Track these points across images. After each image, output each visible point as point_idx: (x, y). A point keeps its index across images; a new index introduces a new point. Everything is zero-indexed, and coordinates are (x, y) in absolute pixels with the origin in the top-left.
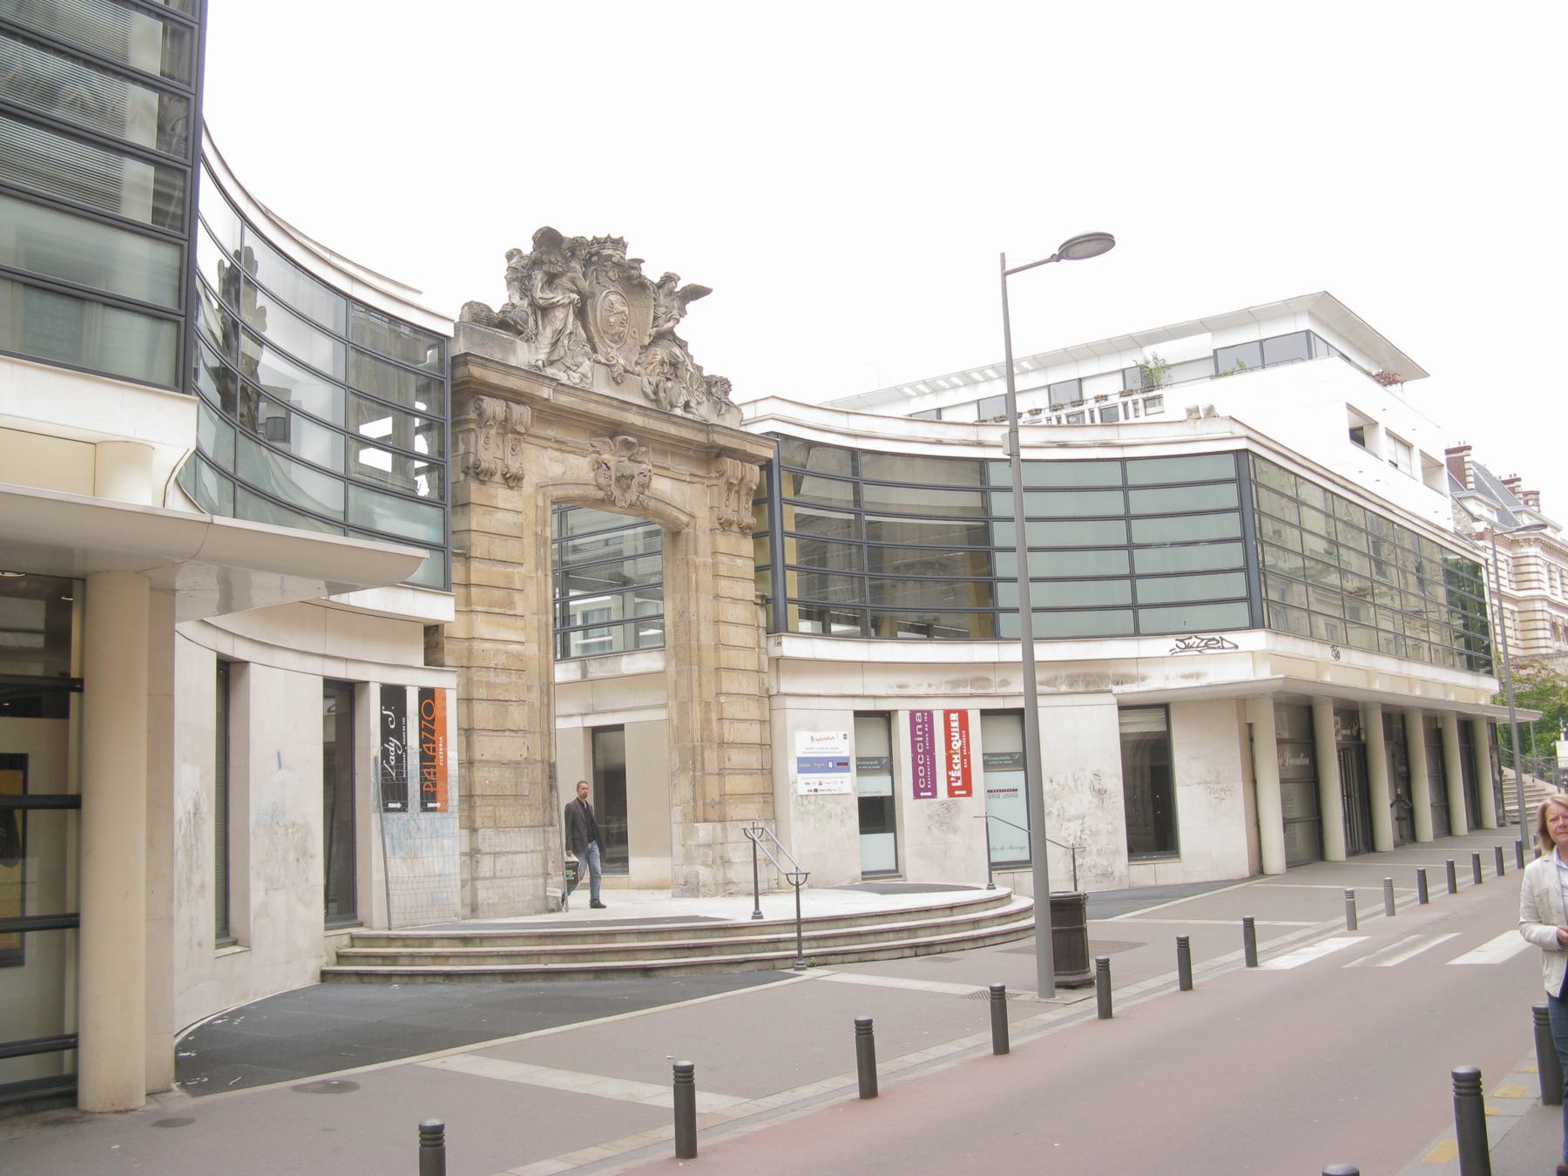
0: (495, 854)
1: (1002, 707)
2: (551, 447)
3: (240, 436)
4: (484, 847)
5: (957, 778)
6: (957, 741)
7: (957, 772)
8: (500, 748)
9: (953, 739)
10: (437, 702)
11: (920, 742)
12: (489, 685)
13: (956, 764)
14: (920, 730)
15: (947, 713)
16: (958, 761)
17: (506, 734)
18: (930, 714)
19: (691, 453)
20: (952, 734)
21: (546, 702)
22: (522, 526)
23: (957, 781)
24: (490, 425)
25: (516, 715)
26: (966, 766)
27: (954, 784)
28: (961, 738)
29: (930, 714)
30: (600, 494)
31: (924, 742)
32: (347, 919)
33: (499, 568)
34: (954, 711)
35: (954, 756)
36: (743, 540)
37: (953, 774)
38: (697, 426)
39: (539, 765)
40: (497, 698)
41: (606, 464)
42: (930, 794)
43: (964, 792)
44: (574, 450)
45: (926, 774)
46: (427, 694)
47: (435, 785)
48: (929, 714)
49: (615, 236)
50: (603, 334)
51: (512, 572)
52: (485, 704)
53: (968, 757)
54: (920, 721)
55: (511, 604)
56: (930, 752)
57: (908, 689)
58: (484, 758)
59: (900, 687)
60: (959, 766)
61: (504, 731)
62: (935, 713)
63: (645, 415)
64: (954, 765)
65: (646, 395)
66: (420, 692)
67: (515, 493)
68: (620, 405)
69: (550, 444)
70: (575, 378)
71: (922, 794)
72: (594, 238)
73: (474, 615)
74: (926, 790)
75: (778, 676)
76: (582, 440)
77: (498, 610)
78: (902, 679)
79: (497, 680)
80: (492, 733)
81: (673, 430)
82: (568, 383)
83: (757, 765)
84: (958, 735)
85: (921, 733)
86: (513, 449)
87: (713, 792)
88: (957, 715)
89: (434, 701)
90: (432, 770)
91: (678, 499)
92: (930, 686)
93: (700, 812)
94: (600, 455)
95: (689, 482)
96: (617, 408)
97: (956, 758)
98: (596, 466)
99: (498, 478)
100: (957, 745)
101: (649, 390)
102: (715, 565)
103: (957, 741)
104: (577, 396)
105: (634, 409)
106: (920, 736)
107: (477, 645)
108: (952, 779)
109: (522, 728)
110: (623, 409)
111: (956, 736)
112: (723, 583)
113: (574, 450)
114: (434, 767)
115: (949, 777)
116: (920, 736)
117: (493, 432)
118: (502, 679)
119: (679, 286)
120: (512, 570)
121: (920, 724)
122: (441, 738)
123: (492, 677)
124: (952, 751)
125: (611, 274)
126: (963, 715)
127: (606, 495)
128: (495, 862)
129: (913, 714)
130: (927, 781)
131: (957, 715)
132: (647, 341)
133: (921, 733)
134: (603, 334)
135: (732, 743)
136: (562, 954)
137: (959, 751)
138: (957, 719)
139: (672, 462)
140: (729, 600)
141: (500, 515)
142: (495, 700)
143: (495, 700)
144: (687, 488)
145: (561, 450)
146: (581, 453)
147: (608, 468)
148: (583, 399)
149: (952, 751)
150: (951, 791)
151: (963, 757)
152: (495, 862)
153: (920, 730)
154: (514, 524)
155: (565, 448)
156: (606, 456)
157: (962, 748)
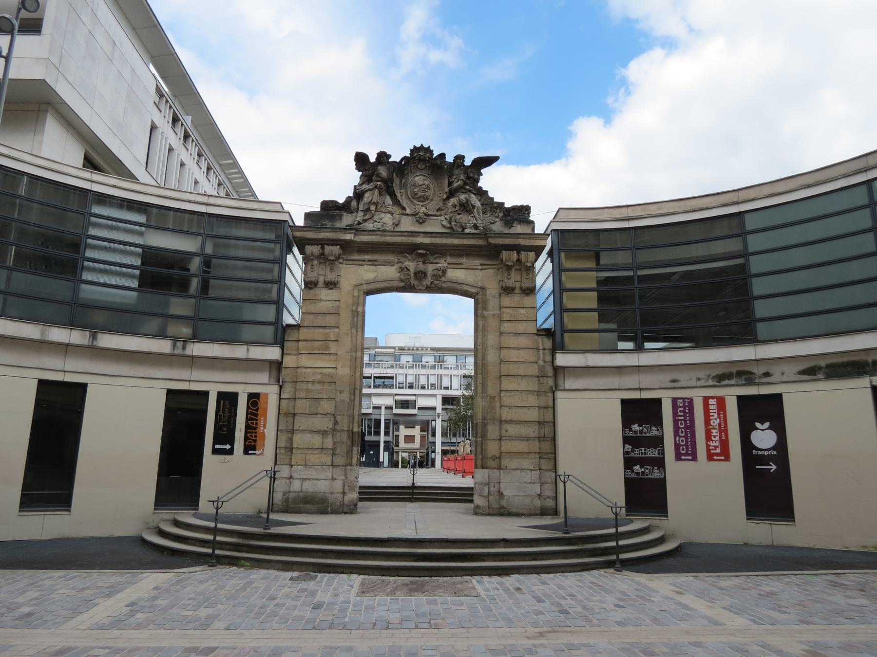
0: (302, 479)
1: (187, 389)
2: (367, 264)
3: (318, 286)
4: (295, 476)
5: (716, 447)
6: (716, 419)
7: (715, 442)
8: (313, 423)
9: (711, 418)
10: (261, 400)
11: (681, 420)
12: (307, 391)
13: (715, 437)
14: (681, 411)
15: (706, 400)
16: (716, 434)
17: (318, 416)
18: (691, 400)
19: (483, 253)
20: (711, 414)
21: (352, 399)
22: (339, 307)
23: (715, 449)
24: (311, 259)
25: (325, 406)
26: (724, 438)
27: (712, 451)
28: (719, 417)
29: (691, 400)
30: (402, 284)
31: (685, 420)
32: (661, 513)
33: (321, 330)
34: (712, 398)
35: (712, 431)
36: (526, 297)
37: (711, 443)
38: (476, 236)
39: (346, 432)
40: (313, 397)
41: (406, 268)
42: (690, 458)
43: (723, 458)
44: (383, 263)
45: (687, 443)
46: (254, 399)
47: (255, 441)
48: (690, 402)
49: (426, 146)
50: (412, 199)
51: (329, 332)
52: (304, 401)
53: (726, 431)
54: (681, 405)
55: (328, 348)
56: (691, 427)
57: (680, 383)
58: (300, 428)
59: (674, 381)
60: (717, 438)
61: (317, 414)
62: (727, 399)
63: (433, 237)
64: (713, 437)
65: (444, 226)
66: (672, 401)
67: (334, 291)
68: (410, 234)
69: (365, 263)
70: (378, 225)
71: (683, 457)
72: (433, 151)
73: (300, 356)
74: (687, 454)
75: (564, 380)
76: (391, 257)
77: (317, 352)
78: (675, 376)
79: (313, 388)
80: (307, 415)
81: (466, 242)
82: (374, 229)
83: (536, 434)
84: (716, 416)
85: (682, 414)
86: (331, 269)
87: (492, 449)
88: (715, 400)
89: (259, 400)
90: (254, 434)
91: (471, 280)
92: (699, 379)
93: (479, 462)
94: (403, 263)
95: (481, 269)
96: (409, 236)
97: (715, 432)
98: (400, 270)
99: (517, 291)
100: (715, 422)
101: (445, 223)
102: (500, 315)
103: (716, 419)
104: (377, 235)
105: (421, 235)
106: (681, 416)
107: (299, 370)
108: (711, 448)
109: (329, 413)
110: (413, 236)
111: (714, 415)
112: (505, 325)
113: (383, 263)
114: (256, 433)
115: (708, 446)
116: (681, 416)
117: (316, 262)
118: (318, 387)
119: (468, 162)
120: (329, 330)
121: (681, 407)
122: (262, 418)
123: (310, 386)
124: (711, 427)
125: (419, 166)
126: (721, 401)
127: (407, 284)
128: (302, 483)
129: (674, 401)
130: (687, 448)
131: (715, 400)
132: (445, 197)
133: (682, 414)
134: (412, 199)
135: (511, 421)
136: (461, 542)
137: (717, 427)
138: (716, 403)
139: (466, 260)
140: (512, 334)
141: (322, 303)
142: (312, 398)
143: (312, 398)
144: (480, 273)
145: (375, 265)
146: (390, 264)
147: (408, 270)
148: (381, 236)
149: (711, 427)
150: (710, 457)
151: (721, 431)
152: (302, 483)
153: (681, 411)
154: (332, 307)
155: (376, 263)
156: (407, 264)
157: (720, 424)
